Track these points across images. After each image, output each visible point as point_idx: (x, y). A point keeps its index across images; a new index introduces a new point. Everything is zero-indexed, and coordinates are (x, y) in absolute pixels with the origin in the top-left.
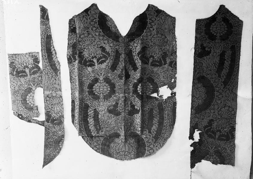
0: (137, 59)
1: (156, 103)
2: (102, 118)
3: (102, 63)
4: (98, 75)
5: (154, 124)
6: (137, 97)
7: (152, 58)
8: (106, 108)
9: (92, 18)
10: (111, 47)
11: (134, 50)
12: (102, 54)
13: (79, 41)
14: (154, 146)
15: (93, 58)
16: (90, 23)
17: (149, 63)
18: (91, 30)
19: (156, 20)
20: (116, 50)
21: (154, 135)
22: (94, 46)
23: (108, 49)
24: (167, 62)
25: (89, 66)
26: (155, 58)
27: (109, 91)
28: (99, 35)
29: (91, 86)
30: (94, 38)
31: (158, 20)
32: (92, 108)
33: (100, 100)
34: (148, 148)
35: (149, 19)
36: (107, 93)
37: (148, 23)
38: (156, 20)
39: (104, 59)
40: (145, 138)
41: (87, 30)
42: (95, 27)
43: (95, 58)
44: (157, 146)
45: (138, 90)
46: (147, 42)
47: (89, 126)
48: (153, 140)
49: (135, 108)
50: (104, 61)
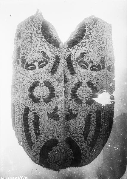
0: (76, 64)
1: (94, 109)
2: (42, 122)
3: (41, 67)
4: (82, 79)
5: (91, 131)
6: (75, 101)
7: (91, 63)
8: (47, 112)
9: (36, 25)
10: (51, 52)
11: (73, 56)
12: (43, 59)
13: (22, 46)
14: (89, 155)
15: (34, 61)
16: (33, 29)
17: (88, 68)
18: (34, 36)
19: (93, 27)
20: (56, 55)
21: (89, 143)
22: (36, 50)
23: (49, 54)
24: (106, 67)
25: (30, 70)
26: (94, 63)
27: (48, 95)
28: (41, 41)
29: (74, 91)
30: (36, 43)
31: (96, 28)
32: (32, 111)
33: (40, 103)
34: (83, 157)
35: (88, 28)
36: (47, 97)
37: (86, 31)
38: (93, 27)
39: (44, 63)
40: (80, 145)
41: (31, 36)
42: (37, 33)
43: (36, 62)
44: (92, 156)
45: (76, 95)
46: (86, 48)
47: (29, 130)
48: (88, 148)
49: (72, 113)
50: (44, 65)
